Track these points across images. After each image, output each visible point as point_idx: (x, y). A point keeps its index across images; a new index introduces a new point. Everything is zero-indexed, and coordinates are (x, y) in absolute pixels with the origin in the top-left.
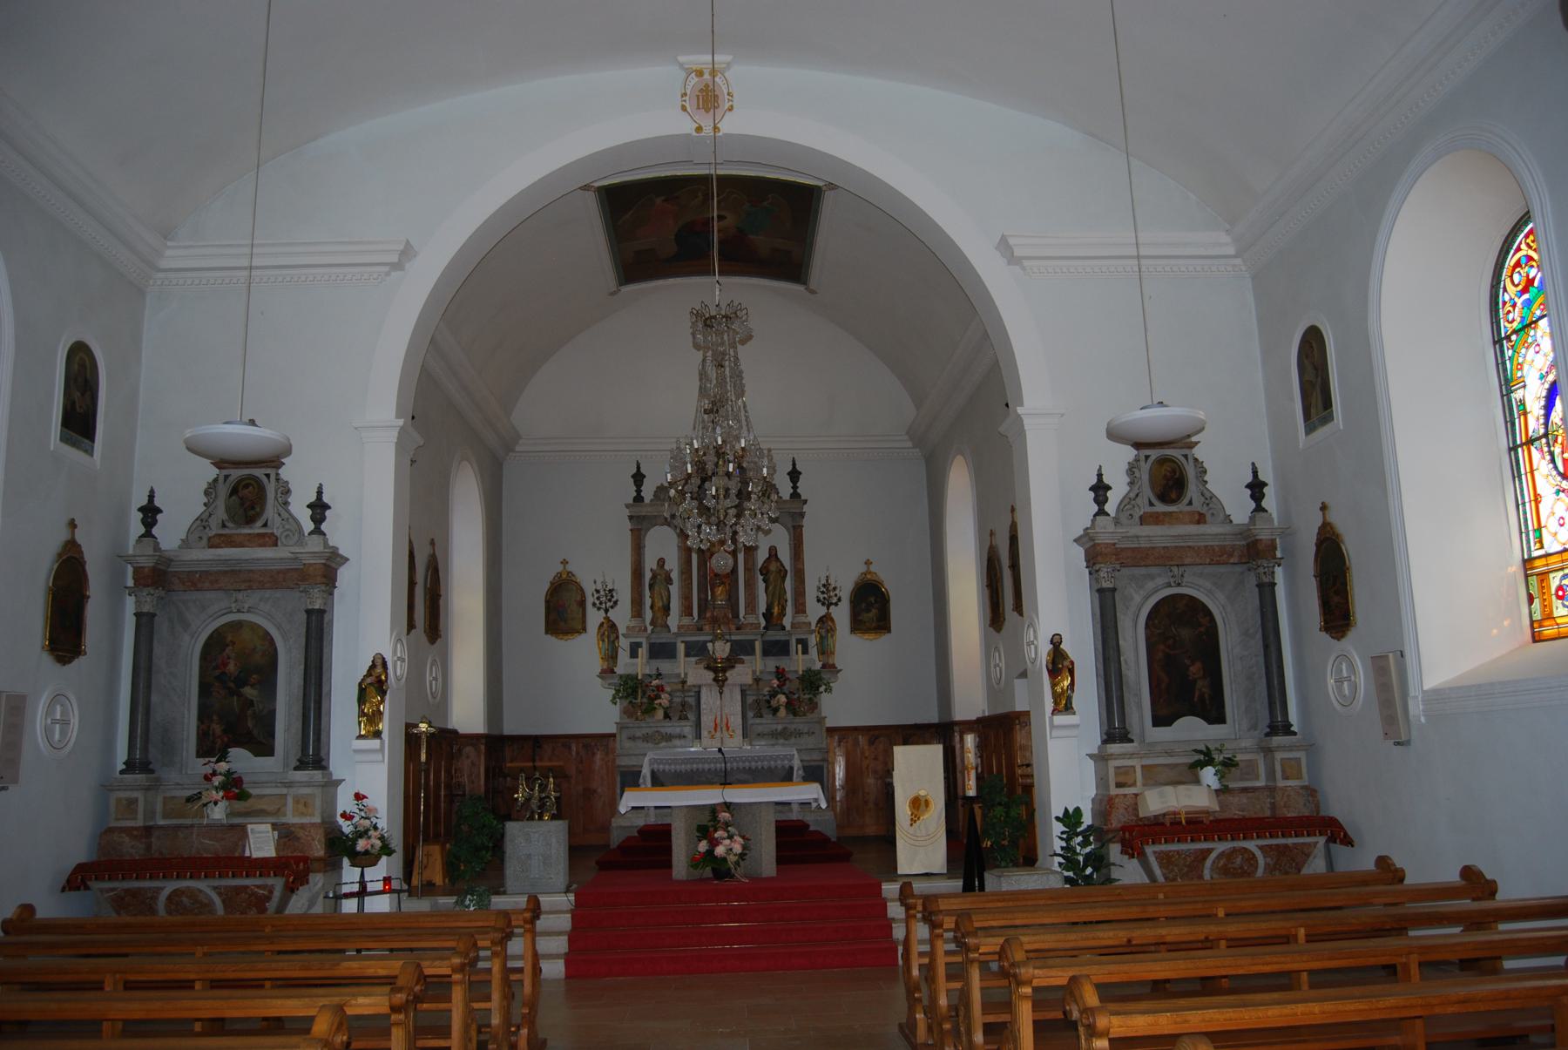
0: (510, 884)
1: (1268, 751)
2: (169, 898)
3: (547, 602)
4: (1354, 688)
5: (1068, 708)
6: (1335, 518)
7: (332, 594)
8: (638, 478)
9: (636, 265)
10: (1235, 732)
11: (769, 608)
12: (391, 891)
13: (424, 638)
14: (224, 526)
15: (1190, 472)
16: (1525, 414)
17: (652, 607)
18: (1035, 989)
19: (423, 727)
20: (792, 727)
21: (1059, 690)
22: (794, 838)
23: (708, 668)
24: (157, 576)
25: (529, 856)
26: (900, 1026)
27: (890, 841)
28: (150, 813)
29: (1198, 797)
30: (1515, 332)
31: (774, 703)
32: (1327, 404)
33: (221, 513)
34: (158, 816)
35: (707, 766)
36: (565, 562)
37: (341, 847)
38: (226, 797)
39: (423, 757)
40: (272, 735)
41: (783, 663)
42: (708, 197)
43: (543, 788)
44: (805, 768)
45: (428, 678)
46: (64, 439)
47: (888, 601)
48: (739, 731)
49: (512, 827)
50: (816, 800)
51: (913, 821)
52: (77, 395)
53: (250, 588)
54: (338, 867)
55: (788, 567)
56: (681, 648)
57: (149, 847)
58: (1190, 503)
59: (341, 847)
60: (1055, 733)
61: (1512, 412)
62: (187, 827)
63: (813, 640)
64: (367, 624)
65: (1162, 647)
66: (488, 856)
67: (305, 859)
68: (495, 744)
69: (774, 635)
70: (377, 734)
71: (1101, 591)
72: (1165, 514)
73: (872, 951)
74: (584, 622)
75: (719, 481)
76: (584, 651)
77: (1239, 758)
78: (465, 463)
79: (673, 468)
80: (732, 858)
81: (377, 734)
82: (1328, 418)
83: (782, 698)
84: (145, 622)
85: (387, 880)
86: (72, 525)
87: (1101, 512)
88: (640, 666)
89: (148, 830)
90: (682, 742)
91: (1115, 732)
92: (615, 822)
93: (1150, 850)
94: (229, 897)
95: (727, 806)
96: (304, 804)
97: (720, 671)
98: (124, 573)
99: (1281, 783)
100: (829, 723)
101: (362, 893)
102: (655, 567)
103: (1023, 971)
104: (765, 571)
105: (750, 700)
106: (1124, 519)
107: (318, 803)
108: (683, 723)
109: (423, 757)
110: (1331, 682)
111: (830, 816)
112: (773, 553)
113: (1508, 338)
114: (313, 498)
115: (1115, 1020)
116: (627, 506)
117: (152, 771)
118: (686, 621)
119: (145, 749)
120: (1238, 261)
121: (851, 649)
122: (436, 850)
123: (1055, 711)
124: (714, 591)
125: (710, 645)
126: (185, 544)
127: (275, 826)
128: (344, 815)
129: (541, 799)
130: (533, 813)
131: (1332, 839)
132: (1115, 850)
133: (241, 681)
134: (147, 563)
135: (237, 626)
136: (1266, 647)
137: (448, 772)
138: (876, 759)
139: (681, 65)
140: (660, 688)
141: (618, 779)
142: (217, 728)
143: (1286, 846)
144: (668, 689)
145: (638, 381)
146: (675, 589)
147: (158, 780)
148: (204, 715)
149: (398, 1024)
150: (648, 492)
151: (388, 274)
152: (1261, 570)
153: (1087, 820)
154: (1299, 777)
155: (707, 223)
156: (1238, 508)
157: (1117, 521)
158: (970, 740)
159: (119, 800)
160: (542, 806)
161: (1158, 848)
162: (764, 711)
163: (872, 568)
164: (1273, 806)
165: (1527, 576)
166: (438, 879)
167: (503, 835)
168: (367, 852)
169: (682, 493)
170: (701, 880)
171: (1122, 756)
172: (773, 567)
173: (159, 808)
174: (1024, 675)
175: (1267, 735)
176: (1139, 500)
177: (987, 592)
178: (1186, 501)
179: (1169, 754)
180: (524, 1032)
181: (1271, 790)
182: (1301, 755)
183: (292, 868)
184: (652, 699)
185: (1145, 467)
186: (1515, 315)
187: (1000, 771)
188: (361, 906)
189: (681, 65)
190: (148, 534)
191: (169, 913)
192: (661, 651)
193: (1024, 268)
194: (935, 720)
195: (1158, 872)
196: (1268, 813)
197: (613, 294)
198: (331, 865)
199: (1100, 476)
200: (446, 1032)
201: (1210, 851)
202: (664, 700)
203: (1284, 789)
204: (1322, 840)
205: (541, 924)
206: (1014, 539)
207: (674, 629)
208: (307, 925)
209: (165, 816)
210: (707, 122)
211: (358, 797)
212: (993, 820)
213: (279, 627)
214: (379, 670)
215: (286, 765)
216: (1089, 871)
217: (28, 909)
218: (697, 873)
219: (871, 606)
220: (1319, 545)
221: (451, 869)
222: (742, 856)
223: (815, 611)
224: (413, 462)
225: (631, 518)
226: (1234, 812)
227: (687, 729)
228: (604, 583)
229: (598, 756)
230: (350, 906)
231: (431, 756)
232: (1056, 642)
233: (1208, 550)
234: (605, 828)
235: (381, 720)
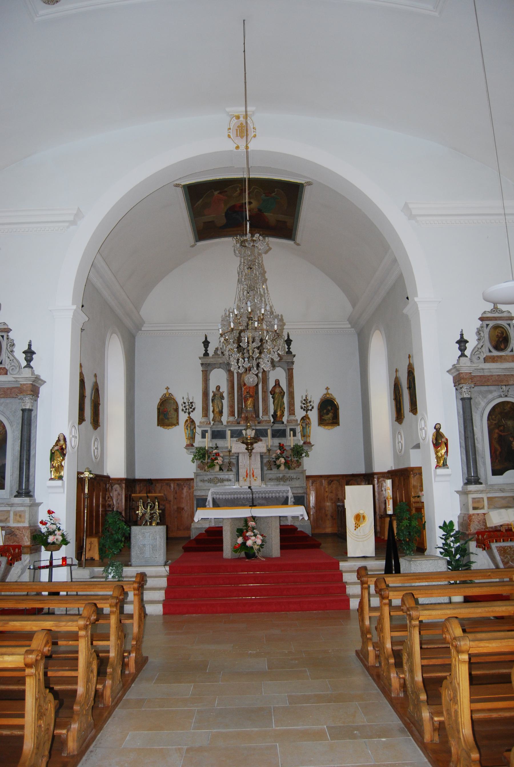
3: (158, 409)
5: (445, 465)
7: (36, 400)
8: (206, 343)
11: (275, 412)
12: (66, 565)
13: (90, 427)
17: (213, 412)
18: (470, 656)
19: (87, 474)
20: (288, 475)
21: (440, 455)
22: (289, 534)
23: (243, 443)
25: (144, 545)
26: (357, 652)
31: (278, 462)
35: (242, 496)
36: (167, 388)
37: (40, 540)
39: (86, 491)
41: (283, 441)
42: (243, 191)
43: (152, 508)
44: (294, 497)
45: (93, 448)
47: (338, 409)
48: (259, 478)
49: (135, 530)
50: (302, 515)
54: (38, 550)
55: (285, 389)
56: (228, 433)
63: (299, 429)
64: (55, 416)
65: (497, 431)
67: (19, 547)
68: (131, 484)
70: (61, 478)
71: (463, 399)
72: (498, 356)
73: (332, 598)
74: (178, 420)
76: (178, 434)
79: (223, 325)
80: (256, 547)
81: (61, 478)
83: (282, 460)
85: (64, 559)
87: (463, 355)
88: (207, 443)
90: (229, 483)
91: (472, 479)
92: (193, 526)
95: (254, 518)
96: (19, 516)
97: (249, 444)
100: (308, 473)
102: (215, 390)
103: (462, 643)
104: (273, 393)
105: (265, 461)
106: (475, 359)
107: (27, 516)
108: (230, 473)
109: (86, 491)
112: (277, 383)
114: (26, 348)
116: (200, 358)
118: (231, 419)
121: (319, 434)
122: (95, 541)
123: (437, 466)
124: (246, 397)
125: (244, 432)
128: (42, 522)
129: (151, 514)
130: (146, 522)
132: (472, 546)
137: (104, 498)
138: (331, 492)
141: (195, 502)
144: (221, 455)
146: (225, 402)
149: (30, 676)
150: (211, 351)
153: (456, 528)
155: (243, 206)
158: (389, 483)
160: (152, 518)
161: (502, 544)
162: (273, 467)
163: (330, 392)
166: (97, 557)
167: (130, 534)
168: (54, 543)
170: (239, 559)
171: (476, 492)
172: (277, 390)
174: (418, 446)
176: (483, 349)
177: (393, 402)
178: (509, 349)
179: (502, 490)
180: (133, 655)
184: (213, 460)
185: (487, 331)
192: (218, 435)
194: (363, 472)
195: (498, 558)
197: (193, 246)
198: (34, 550)
199: (462, 335)
202: (220, 460)
206: (411, 373)
207: (225, 423)
210: (242, 143)
211: (50, 512)
213: (8, 419)
214: (62, 442)
215: (11, 494)
216: (458, 556)
218: (237, 555)
219: (329, 411)
221: (102, 551)
222: (262, 546)
223: (300, 414)
224: (82, 330)
225: (202, 364)
227: (232, 476)
228: (188, 399)
229: (185, 490)
231: (93, 489)
234: (189, 528)
235: (62, 470)
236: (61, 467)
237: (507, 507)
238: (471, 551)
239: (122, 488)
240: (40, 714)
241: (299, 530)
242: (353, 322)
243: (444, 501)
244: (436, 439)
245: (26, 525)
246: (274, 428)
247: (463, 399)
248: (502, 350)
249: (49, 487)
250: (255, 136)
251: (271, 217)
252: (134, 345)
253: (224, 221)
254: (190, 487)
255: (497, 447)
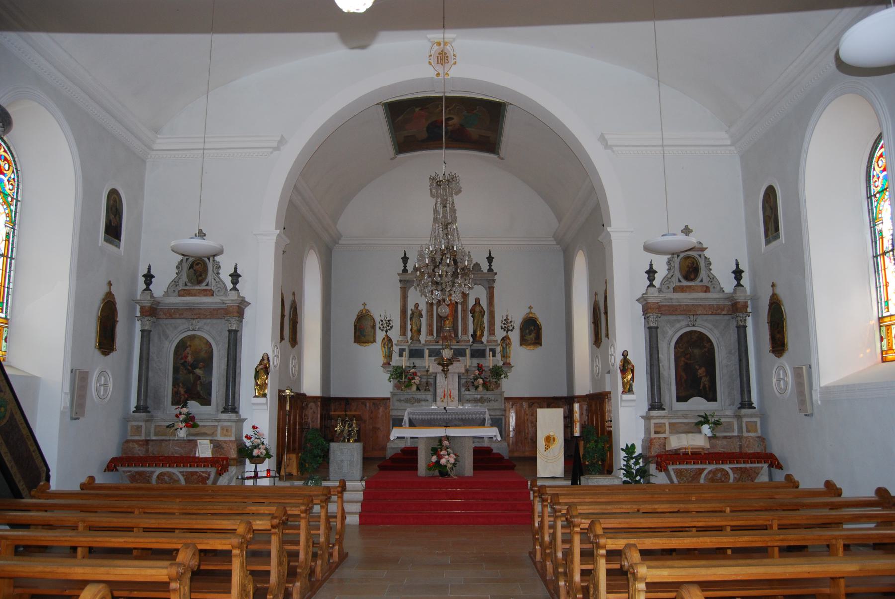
0: (332, 475)
1: (739, 417)
2: (158, 477)
3: (355, 326)
4: (786, 384)
5: (630, 391)
6: (778, 291)
8: (405, 259)
9: (405, 143)
10: (722, 406)
11: (475, 332)
12: (270, 477)
14: (186, 285)
15: (702, 264)
16: (882, 238)
19: (288, 392)
21: (625, 380)
22: (484, 457)
23: (439, 364)
24: (152, 311)
25: (342, 461)
27: (534, 460)
28: (148, 433)
29: (698, 441)
30: (878, 193)
31: (476, 383)
32: (777, 229)
33: (185, 278)
34: (152, 434)
36: (365, 304)
37: (245, 453)
38: (187, 426)
40: (210, 395)
41: (482, 361)
43: (350, 426)
44: (491, 419)
45: (291, 366)
46: (106, 240)
47: (541, 329)
48: (457, 398)
49: (333, 446)
51: (546, 449)
52: (112, 216)
53: (199, 318)
54: (243, 464)
55: (485, 309)
56: (426, 352)
57: (147, 451)
58: (701, 281)
59: (245, 453)
60: (623, 404)
61: (876, 236)
62: (166, 441)
63: (498, 350)
64: (259, 338)
65: (683, 359)
66: (321, 460)
67: (227, 459)
68: (326, 401)
69: (477, 346)
70: (264, 395)
71: (650, 328)
72: (687, 287)
74: (375, 337)
75: (446, 266)
76: (374, 353)
77: (722, 420)
78: (312, 251)
79: (419, 261)
80: (449, 466)
81: (264, 395)
82: (777, 237)
83: (481, 381)
84: (146, 335)
85: (268, 471)
86: (110, 284)
87: (651, 285)
88: (404, 362)
89: (147, 442)
92: (389, 445)
93: (670, 468)
94: (188, 477)
95: (447, 438)
96: (226, 430)
97: (445, 365)
98: (135, 308)
99: (745, 434)
100: (506, 395)
101: (256, 477)
104: (473, 311)
105: (463, 381)
107: (233, 430)
110: (774, 380)
111: (505, 445)
112: (478, 302)
113: (875, 196)
114: (232, 271)
115: (609, 541)
117: (149, 412)
118: (429, 337)
119: (146, 400)
120: (733, 148)
121: (520, 355)
126: (166, 294)
127: (211, 442)
131: (771, 466)
132: (653, 468)
133: (194, 366)
134: (147, 304)
135: (192, 337)
136: (740, 360)
137: (301, 416)
139: (429, 40)
140: (415, 374)
142: (182, 390)
143: (746, 468)
144: (419, 374)
145: (402, 209)
146: (424, 321)
147: (152, 416)
148: (175, 383)
149: (275, 534)
150: (410, 268)
151: (272, 153)
152: (739, 318)
153: (638, 451)
154: (756, 431)
156: (728, 284)
157: (660, 290)
159: (132, 426)
160: (349, 435)
161: (675, 467)
162: (471, 388)
163: (532, 311)
164: (741, 447)
165: (880, 326)
166: (295, 472)
168: (258, 456)
169: (422, 274)
170: (433, 477)
172: (478, 309)
173: (152, 430)
174: (609, 372)
175: (740, 408)
179: (685, 417)
180: (336, 548)
181: (740, 438)
182: (757, 420)
183: (220, 463)
184: (410, 380)
186: (879, 183)
187: (597, 423)
188: (255, 483)
189: (429, 40)
190: (147, 289)
191: (157, 482)
192: (416, 354)
193: (613, 151)
195: (675, 480)
196: (738, 451)
197: (392, 159)
198: (240, 463)
199: (651, 265)
200: (297, 543)
201: (703, 469)
202: (417, 380)
203: (747, 438)
204: (765, 466)
205: (346, 495)
206: (606, 298)
207: (423, 342)
208: (229, 491)
209: (156, 435)
210: (440, 68)
211: (254, 427)
212: (589, 449)
213: (214, 338)
214: (265, 362)
215: (217, 410)
216: (638, 478)
217: (92, 479)
218: (431, 473)
219: (532, 331)
220: (771, 305)
221: (301, 467)
222: (455, 464)
223: (499, 334)
224: (284, 252)
225: (401, 281)
226: (719, 450)
229: (381, 410)
230: (249, 483)
231: (292, 406)
232: (625, 355)
233: (711, 307)
234: (384, 449)
236: (265, 385)
237: (687, 433)
238: (651, 472)
239: (317, 406)
240: (280, 563)
241: (495, 451)
242: (559, 239)
243: (630, 424)
244: (623, 366)
245: (233, 439)
246: (473, 348)
247: (650, 328)
248: (692, 280)
249: (253, 404)
250: (455, 63)
251: (474, 132)
252: (331, 257)
253: (425, 135)
254: (387, 407)
255: (683, 374)
